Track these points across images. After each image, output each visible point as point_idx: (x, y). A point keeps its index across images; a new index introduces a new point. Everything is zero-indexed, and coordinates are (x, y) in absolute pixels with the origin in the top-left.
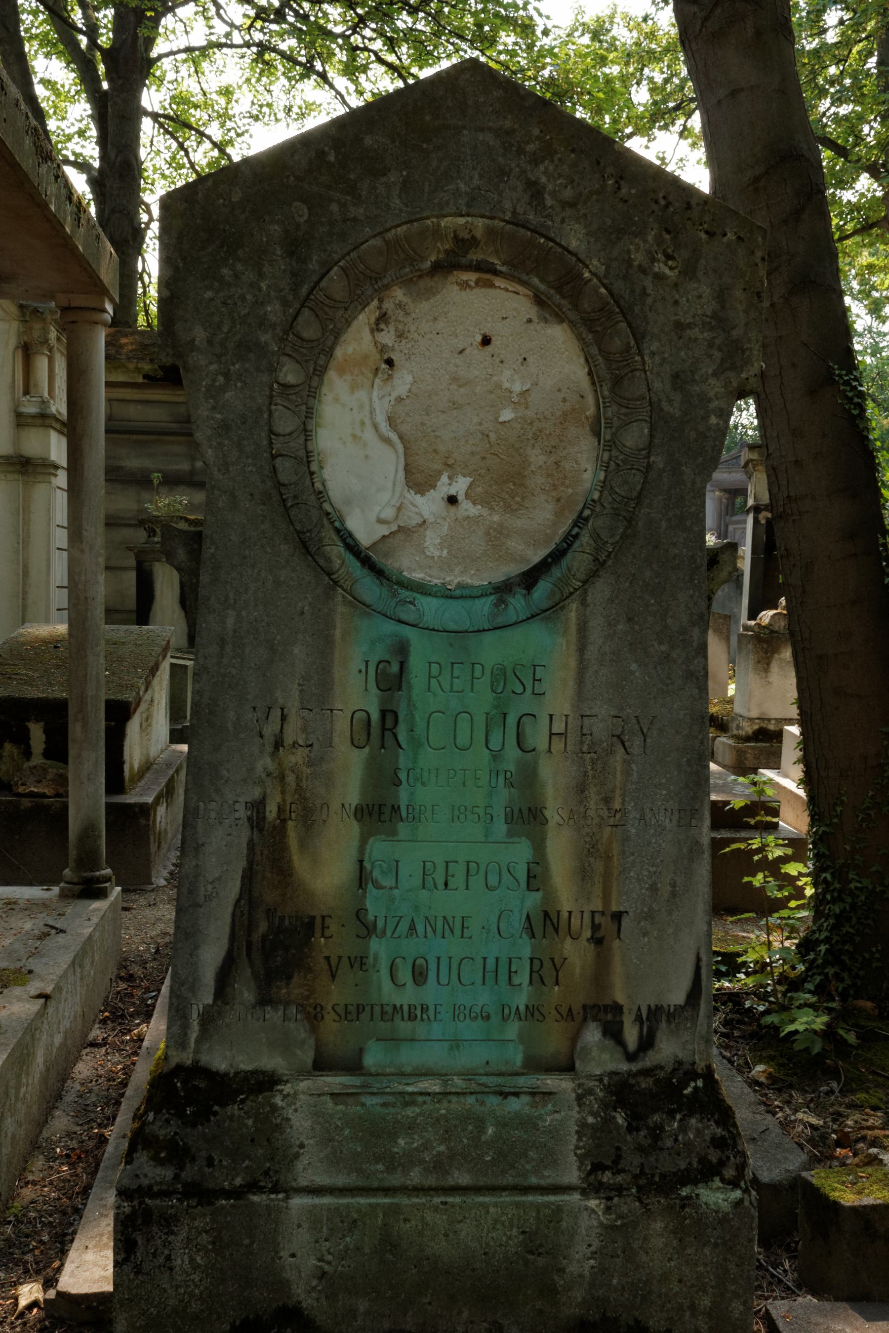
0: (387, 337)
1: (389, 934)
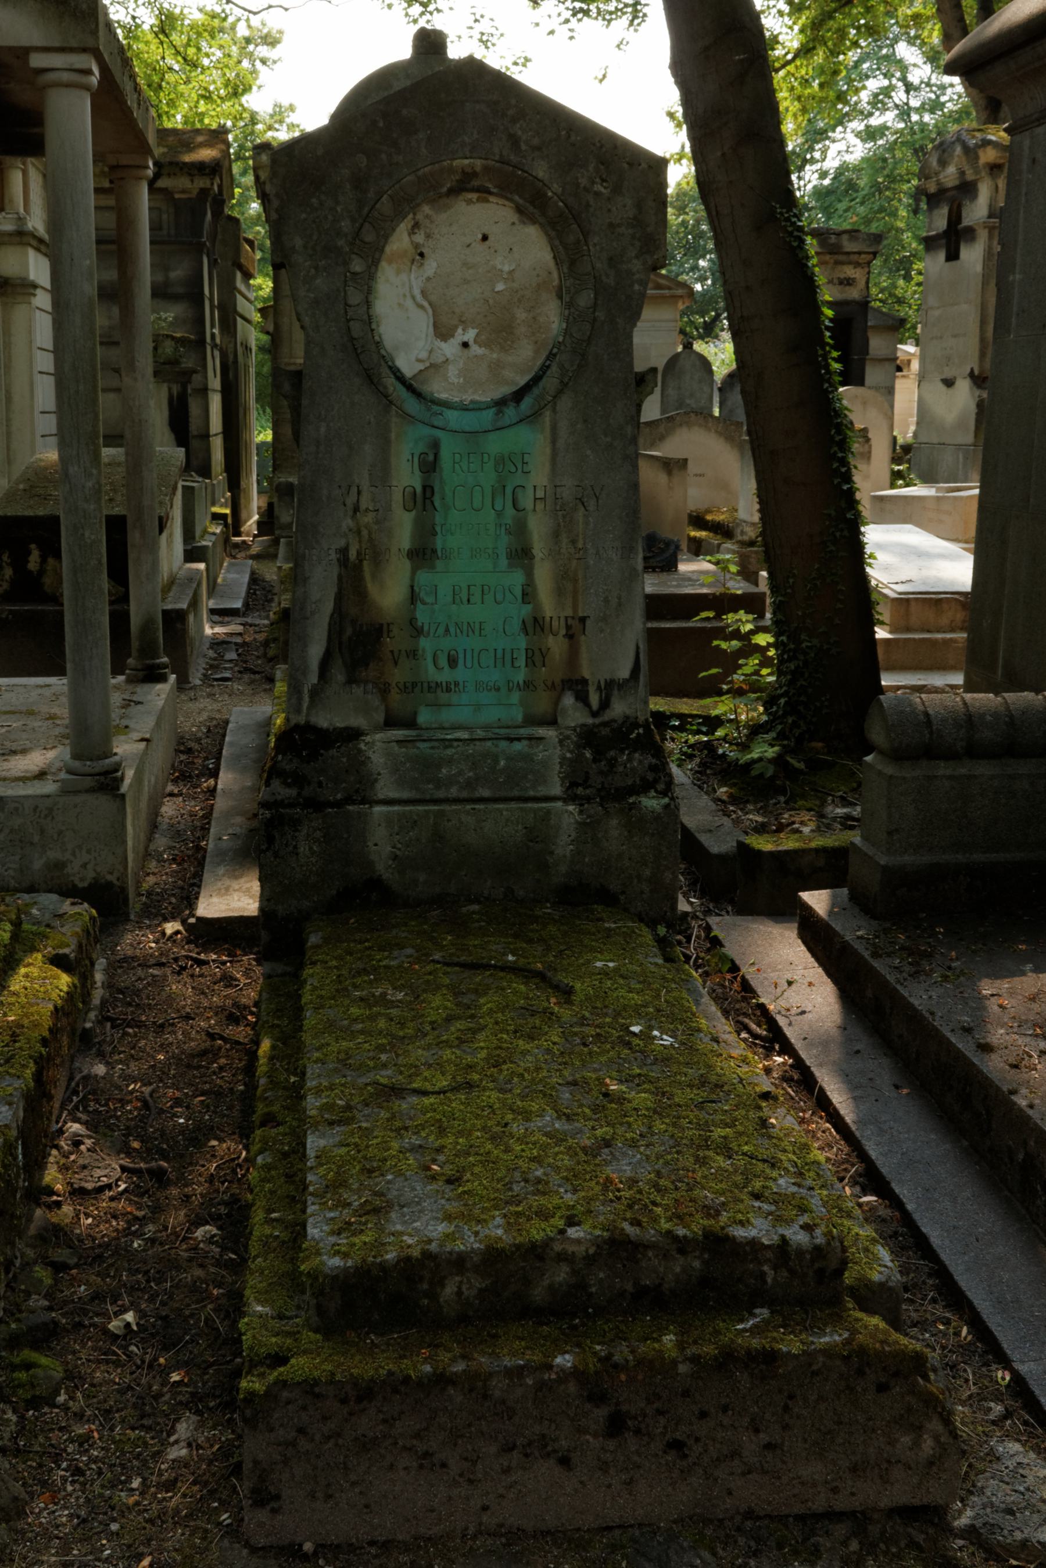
0: (419, 238)
1: (432, 634)
